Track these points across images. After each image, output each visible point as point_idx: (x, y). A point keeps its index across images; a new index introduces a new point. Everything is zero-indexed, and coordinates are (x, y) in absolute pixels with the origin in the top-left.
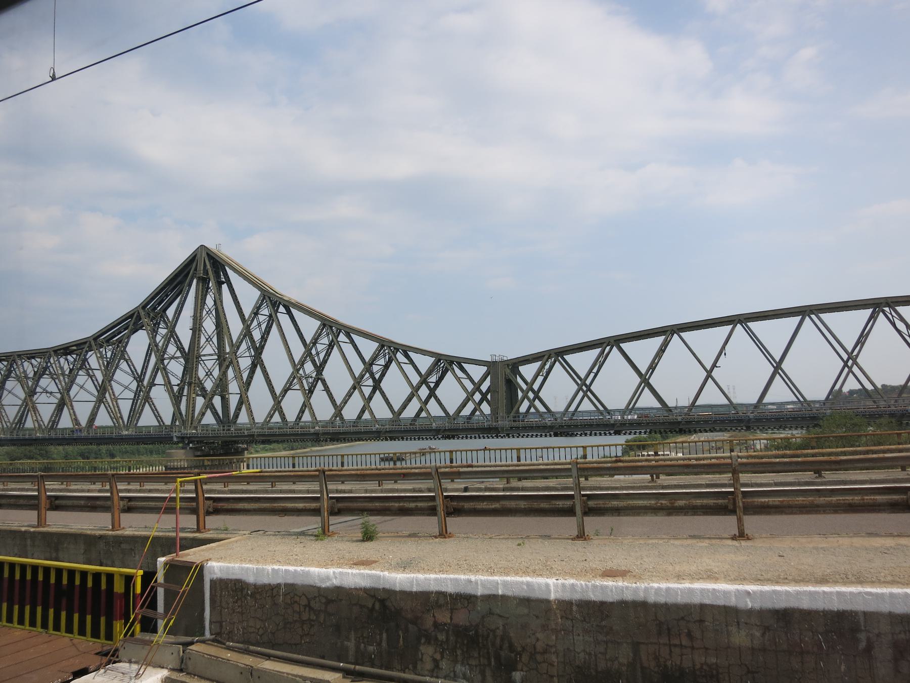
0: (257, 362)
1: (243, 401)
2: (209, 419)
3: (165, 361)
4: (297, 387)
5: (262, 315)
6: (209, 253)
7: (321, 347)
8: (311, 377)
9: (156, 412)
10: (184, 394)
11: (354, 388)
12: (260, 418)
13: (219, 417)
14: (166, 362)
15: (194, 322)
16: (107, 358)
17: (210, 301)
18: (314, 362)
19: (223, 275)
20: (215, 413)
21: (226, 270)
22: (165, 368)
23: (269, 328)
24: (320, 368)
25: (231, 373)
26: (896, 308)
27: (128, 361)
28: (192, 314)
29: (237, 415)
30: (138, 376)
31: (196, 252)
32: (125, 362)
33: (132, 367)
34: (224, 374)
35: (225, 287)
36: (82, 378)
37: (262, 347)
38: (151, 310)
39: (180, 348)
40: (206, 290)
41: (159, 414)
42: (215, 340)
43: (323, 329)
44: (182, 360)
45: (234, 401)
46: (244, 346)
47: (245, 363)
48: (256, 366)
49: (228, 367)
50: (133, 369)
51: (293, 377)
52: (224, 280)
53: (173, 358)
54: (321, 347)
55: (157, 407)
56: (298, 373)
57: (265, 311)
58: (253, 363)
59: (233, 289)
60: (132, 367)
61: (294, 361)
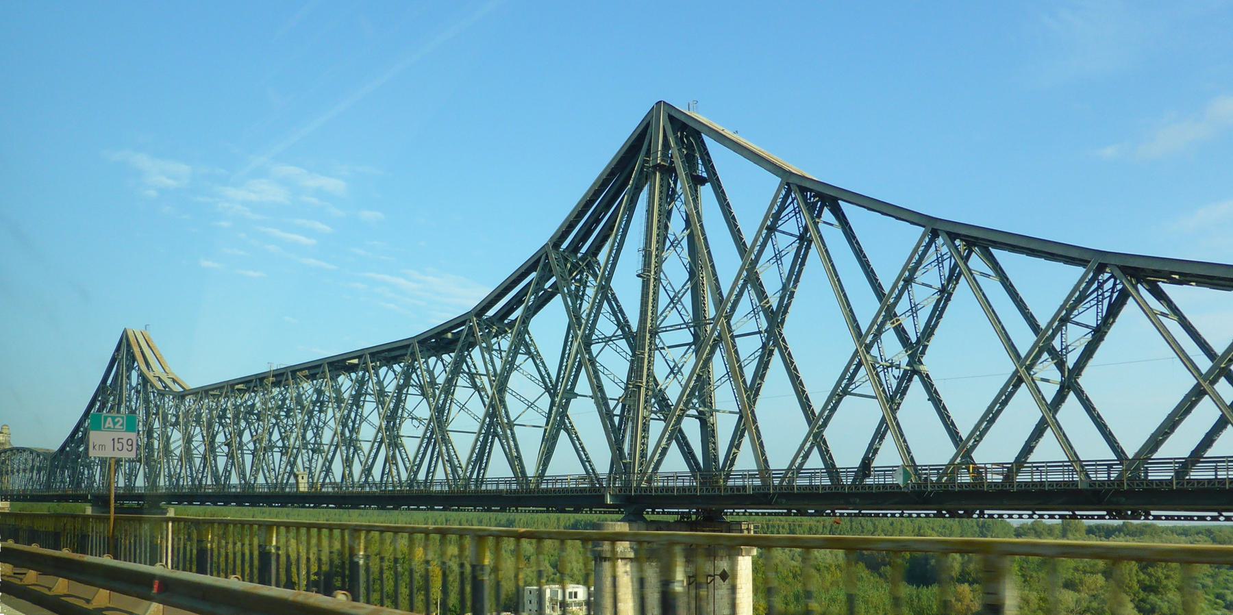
0: (773, 340)
1: (746, 423)
2: (674, 463)
3: (592, 347)
4: (868, 389)
5: (784, 232)
6: (673, 113)
7: (923, 294)
8: (898, 367)
9: (582, 453)
10: (618, 418)
11: (1016, 381)
12: (779, 460)
13: (697, 463)
14: (595, 349)
15: (645, 261)
16: (500, 351)
17: (677, 225)
18: (901, 332)
19: (704, 164)
20: (688, 454)
21: (702, 141)
22: (592, 361)
23: (800, 260)
24: (916, 349)
25: (718, 366)
26: (816, 447)
27: (534, 356)
28: (642, 246)
29: (731, 459)
30: (552, 385)
31: (649, 118)
32: (530, 359)
33: (542, 369)
34: (705, 365)
35: (706, 191)
36: (462, 391)
37: (784, 309)
38: (570, 252)
39: (623, 325)
40: (669, 196)
41: (587, 458)
42: (687, 300)
43: (928, 246)
44: (623, 343)
45: (725, 427)
46: (745, 305)
47: (749, 348)
48: (771, 353)
49: (712, 352)
50: (544, 373)
51: (855, 364)
52: (705, 175)
53: (607, 340)
54: (923, 294)
55: (585, 445)
56: (868, 353)
57: (791, 225)
58: (764, 346)
59: (723, 192)
60: (542, 369)
61: (858, 326)
